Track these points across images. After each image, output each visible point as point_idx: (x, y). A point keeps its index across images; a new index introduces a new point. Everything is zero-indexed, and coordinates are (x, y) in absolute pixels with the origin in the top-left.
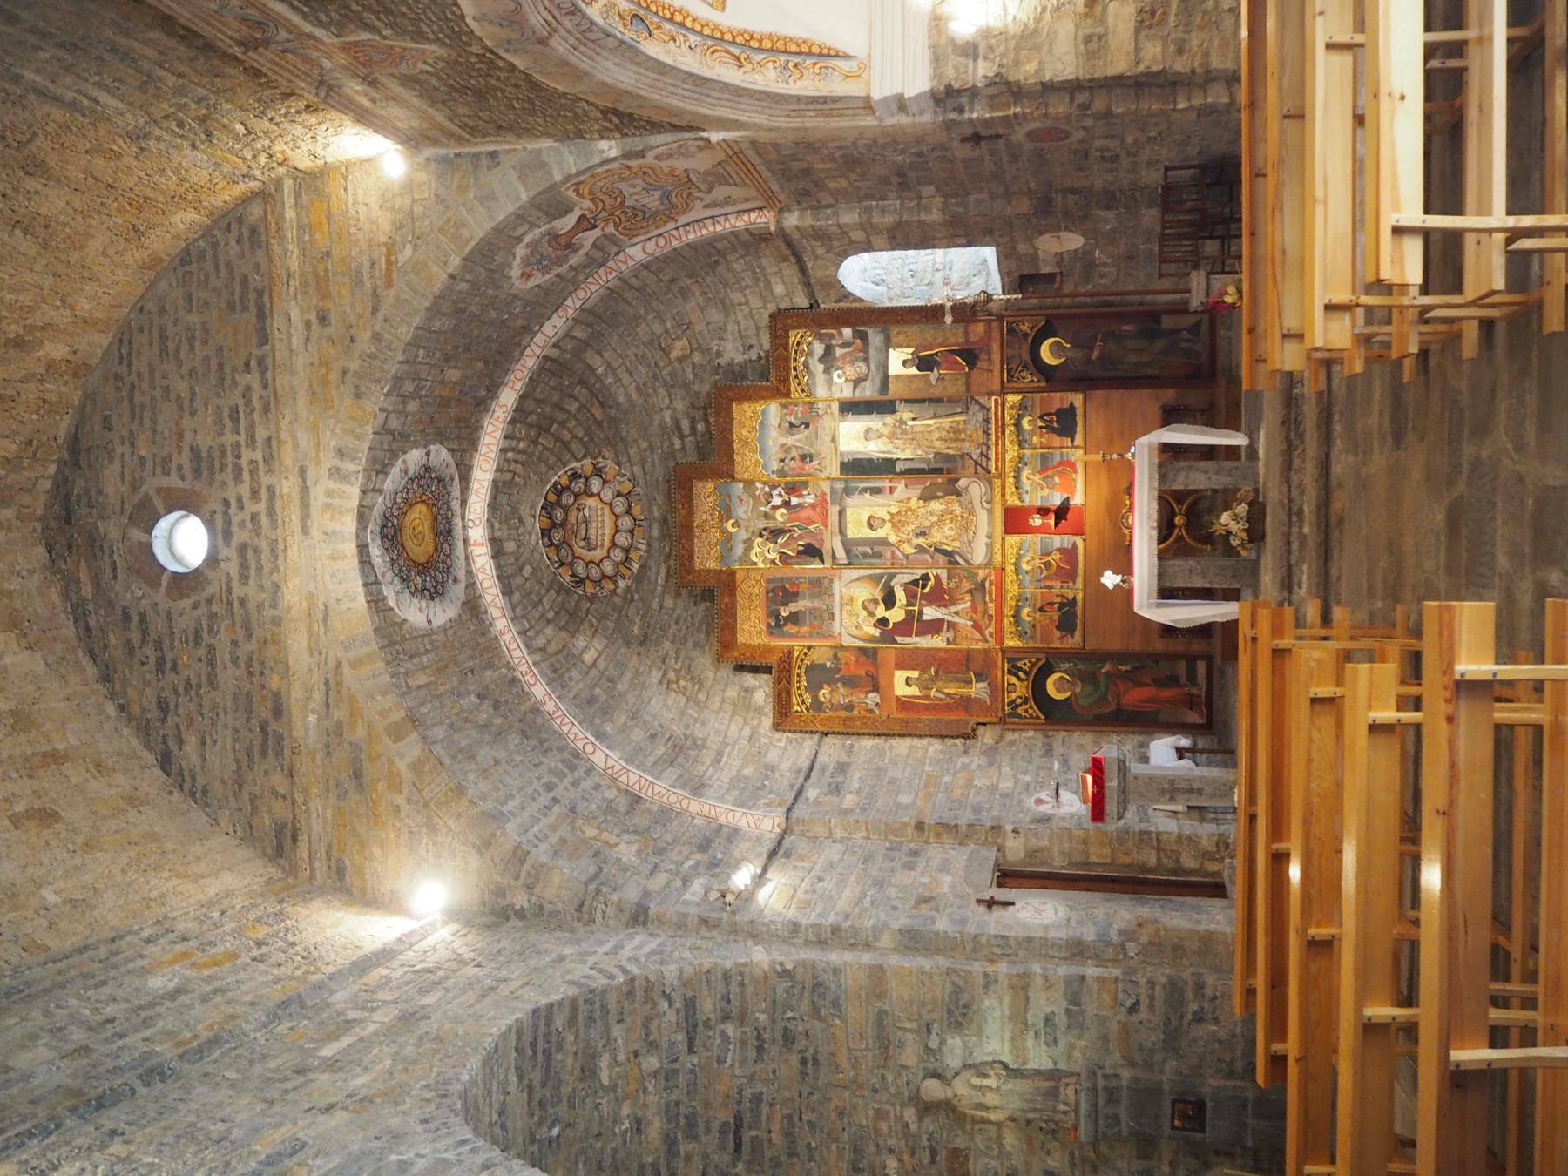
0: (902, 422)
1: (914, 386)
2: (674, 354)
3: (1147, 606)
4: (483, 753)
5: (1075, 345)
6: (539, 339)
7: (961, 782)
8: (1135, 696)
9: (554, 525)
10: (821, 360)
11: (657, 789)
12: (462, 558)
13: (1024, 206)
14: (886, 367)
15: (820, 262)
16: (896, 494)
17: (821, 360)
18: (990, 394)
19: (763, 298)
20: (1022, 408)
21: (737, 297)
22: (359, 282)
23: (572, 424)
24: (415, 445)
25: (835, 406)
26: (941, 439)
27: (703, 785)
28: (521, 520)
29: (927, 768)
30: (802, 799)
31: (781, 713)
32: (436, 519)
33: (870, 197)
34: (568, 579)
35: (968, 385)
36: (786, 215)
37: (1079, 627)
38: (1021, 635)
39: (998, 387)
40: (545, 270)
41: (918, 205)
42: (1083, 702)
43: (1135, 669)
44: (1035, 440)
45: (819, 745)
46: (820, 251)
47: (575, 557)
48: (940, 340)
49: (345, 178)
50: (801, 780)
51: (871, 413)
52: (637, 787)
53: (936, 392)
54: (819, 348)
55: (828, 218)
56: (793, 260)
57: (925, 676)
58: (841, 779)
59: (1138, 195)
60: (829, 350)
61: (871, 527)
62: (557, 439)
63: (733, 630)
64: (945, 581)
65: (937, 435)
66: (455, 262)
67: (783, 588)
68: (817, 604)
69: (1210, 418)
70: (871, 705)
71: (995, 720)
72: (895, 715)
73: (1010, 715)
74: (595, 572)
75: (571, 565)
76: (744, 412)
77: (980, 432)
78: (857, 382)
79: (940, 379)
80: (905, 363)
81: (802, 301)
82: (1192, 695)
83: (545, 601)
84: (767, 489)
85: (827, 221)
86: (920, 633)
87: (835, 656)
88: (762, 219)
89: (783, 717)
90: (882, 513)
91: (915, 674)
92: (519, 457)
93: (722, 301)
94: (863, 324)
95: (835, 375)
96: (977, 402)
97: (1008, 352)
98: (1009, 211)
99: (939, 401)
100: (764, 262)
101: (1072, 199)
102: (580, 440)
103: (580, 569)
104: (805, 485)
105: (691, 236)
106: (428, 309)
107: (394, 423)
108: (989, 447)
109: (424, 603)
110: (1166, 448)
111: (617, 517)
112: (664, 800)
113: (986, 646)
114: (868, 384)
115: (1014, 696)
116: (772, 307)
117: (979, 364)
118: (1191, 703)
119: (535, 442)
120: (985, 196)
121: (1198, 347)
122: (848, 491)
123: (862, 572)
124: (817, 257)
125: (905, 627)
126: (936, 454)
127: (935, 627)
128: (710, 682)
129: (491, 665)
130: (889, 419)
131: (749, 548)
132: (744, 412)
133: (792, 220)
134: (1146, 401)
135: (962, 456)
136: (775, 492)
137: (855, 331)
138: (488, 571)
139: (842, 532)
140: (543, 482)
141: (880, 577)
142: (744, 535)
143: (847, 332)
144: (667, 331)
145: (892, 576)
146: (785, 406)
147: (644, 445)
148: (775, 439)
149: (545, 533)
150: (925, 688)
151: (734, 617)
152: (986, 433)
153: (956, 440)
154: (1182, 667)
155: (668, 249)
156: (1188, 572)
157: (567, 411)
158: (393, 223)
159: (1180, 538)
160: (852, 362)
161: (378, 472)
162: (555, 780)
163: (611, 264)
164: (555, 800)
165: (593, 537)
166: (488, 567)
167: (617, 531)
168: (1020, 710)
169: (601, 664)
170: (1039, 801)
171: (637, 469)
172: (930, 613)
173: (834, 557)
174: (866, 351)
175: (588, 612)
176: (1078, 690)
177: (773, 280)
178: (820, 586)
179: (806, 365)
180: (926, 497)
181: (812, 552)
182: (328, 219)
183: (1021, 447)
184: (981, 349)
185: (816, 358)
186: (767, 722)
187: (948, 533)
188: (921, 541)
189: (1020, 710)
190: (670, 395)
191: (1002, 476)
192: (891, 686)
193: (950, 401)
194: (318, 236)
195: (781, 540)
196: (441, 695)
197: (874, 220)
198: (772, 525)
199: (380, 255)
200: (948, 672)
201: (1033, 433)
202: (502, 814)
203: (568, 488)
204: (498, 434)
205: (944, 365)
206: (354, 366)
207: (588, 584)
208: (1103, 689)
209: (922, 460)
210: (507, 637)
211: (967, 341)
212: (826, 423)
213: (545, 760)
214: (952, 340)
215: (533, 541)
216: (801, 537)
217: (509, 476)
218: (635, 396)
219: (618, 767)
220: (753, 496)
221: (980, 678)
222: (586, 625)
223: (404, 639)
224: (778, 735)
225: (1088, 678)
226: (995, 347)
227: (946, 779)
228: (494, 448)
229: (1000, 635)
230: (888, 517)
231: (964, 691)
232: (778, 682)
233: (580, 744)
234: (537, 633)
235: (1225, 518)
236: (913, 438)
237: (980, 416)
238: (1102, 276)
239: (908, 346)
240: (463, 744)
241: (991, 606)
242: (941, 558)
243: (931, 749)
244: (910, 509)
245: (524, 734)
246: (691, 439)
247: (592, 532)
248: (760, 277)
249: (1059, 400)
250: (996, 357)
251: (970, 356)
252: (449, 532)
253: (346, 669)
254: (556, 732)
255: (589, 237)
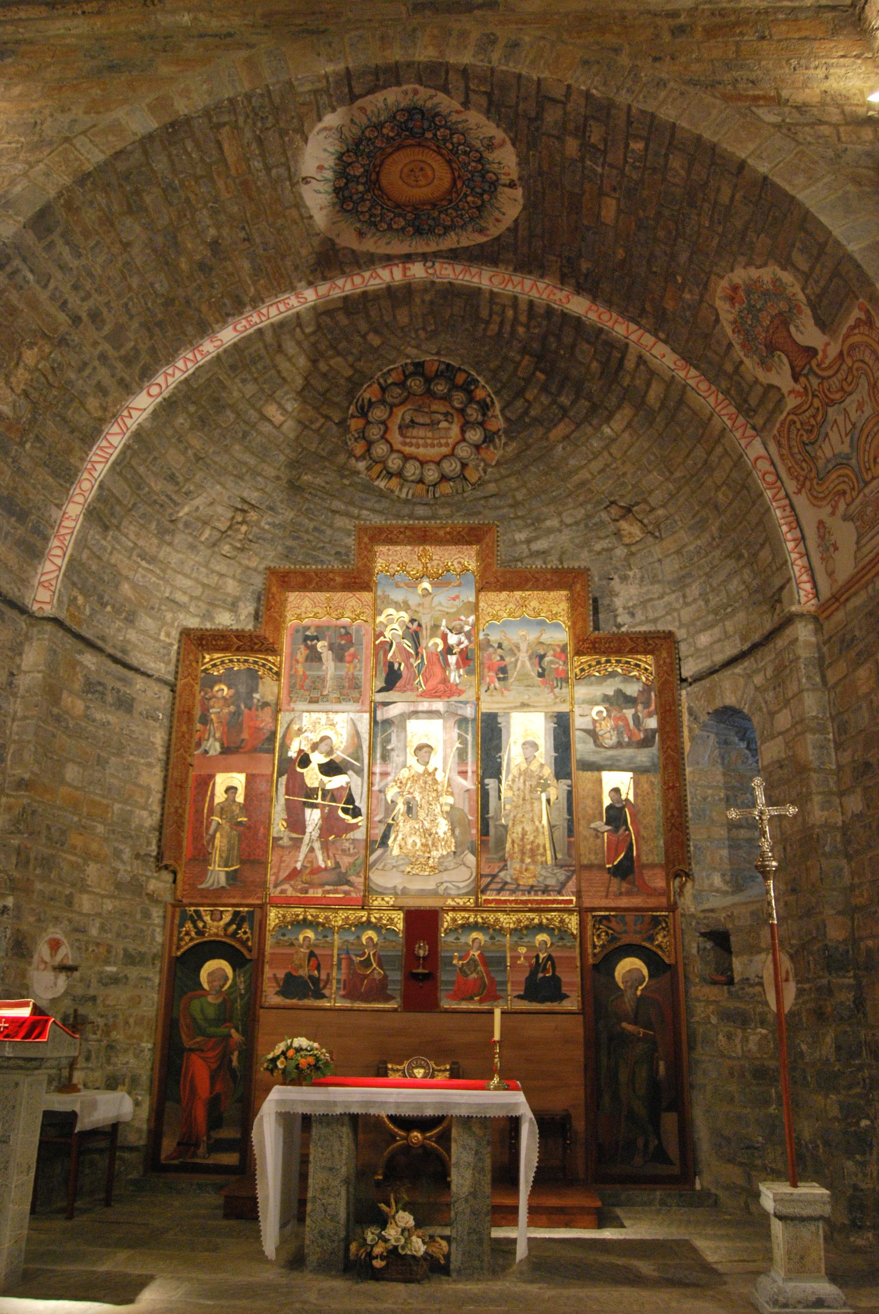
0: (545, 787)
1: (589, 802)
2: (623, 524)
3: (277, 1100)
4: (138, 229)
5: (640, 1000)
6: (648, 339)
7: (94, 846)
8: (199, 1071)
9: (428, 381)
10: (619, 692)
11: (99, 467)
12: (388, 250)
13: (836, 933)
14: (611, 768)
15: (742, 681)
16: (460, 780)
17: (619, 692)
18: (579, 894)
19: (693, 623)
20: (562, 932)
21: (694, 590)
22: (729, 66)
23: (545, 400)
24: (523, 161)
25: (564, 708)
26: (524, 833)
27: (106, 528)
28: (434, 334)
29: (117, 806)
30: (81, 646)
31: (201, 639)
32: (434, 206)
33: (842, 729)
34: (367, 396)
35: (589, 867)
36: (811, 627)
37: (288, 1002)
38: (282, 928)
39: (587, 903)
40: (739, 326)
41: (831, 793)
42: (196, 1005)
43: (232, 1071)
44: (523, 950)
45: (159, 680)
46: (758, 680)
47: (392, 407)
48: (643, 833)
49: (857, 57)
50: (111, 651)
51: (556, 749)
52: (104, 444)
53: (581, 829)
54: (632, 690)
55: (809, 678)
56: (745, 647)
57: (237, 811)
58: (110, 699)
59: (857, 1090)
60: (631, 701)
61: (419, 748)
62: (528, 380)
63: (303, 587)
64: (351, 835)
65: (529, 828)
66: (763, 168)
67: (350, 643)
68: (329, 683)
69: (544, 1179)
70: (206, 745)
71: (179, 894)
72: (192, 773)
73: (184, 912)
74: (374, 432)
75: (383, 402)
76: (557, 603)
77: (531, 882)
78: (592, 733)
79: (597, 834)
80: (616, 791)
81: (689, 669)
82: (197, 1145)
83: (339, 359)
84: (467, 628)
85: (804, 675)
86: (289, 805)
87: (266, 704)
88: (803, 598)
89: (200, 641)
90: (436, 761)
91: (240, 798)
92: (507, 328)
93: (689, 575)
94: (662, 741)
95: (601, 708)
96: (569, 878)
97: (630, 917)
98: (829, 911)
99: (570, 831)
100: (741, 616)
101: (846, 997)
102: (526, 412)
103: (378, 413)
104: (470, 673)
105: (778, 513)
106: (699, 138)
107: (552, 115)
108: (513, 892)
109: (329, 175)
110: (514, 1123)
111: (438, 463)
112: (86, 475)
113: (271, 886)
114: (591, 746)
115: (207, 918)
116: (681, 634)
117: (615, 881)
118: (187, 1144)
119: (524, 351)
120: (847, 880)
121: (638, 1160)
122: (462, 722)
123: (365, 736)
124: (749, 676)
125: (297, 786)
126: (505, 827)
127: (296, 824)
128: (245, 562)
129: (257, 271)
130: (548, 772)
131: (398, 607)
132: (557, 603)
133: (804, 632)
134: (570, 1097)
135: (503, 859)
136: (463, 638)
137: (654, 731)
138: (372, 282)
139: (415, 714)
140: (476, 365)
141: (358, 759)
142: (413, 601)
143: (652, 723)
144: (653, 510)
145: (359, 772)
146: (564, 648)
147: (519, 496)
148: (523, 638)
149: (419, 366)
150: (223, 810)
151: (319, 589)
152: (531, 889)
153: (523, 853)
154: (228, 1133)
155: (762, 485)
156: (334, 1164)
157: (559, 394)
158: (805, 105)
159: (393, 1137)
160: (616, 727)
161: (489, 95)
162: (107, 329)
163: (741, 420)
164: (76, 320)
165: (415, 432)
166: (378, 281)
167: (422, 463)
168: (189, 925)
169: (266, 428)
170: (55, 945)
171: (492, 488)
172: (313, 817)
173: (386, 704)
174: (629, 745)
175: (328, 418)
176: (210, 999)
177: (717, 631)
178: (350, 689)
179: (613, 674)
180: (452, 815)
181: (392, 679)
182: (805, 38)
183: (513, 931)
184: (632, 883)
185: (621, 686)
186: (193, 623)
187: (410, 841)
188: (401, 807)
189: (189, 925)
190: (577, 523)
191: (477, 909)
192: (228, 769)
193: (570, 845)
194: (784, 28)
195: (407, 644)
196: (212, 181)
197: (810, 737)
198: (424, 633)
199: (767, 88)
200: (240, 836)
201: (531, 947)
202: (50, 231)
203: (471, 399)
204: (534, 294)
205: (614, 838)
206: (624, 60)
207: (360, 423)
208: (212, 1030)
209: (498, 810)
210: (293, 301)
211: (644, 866)
212: (545, 696)
213: (135, 325)
214: (645, 848)
215: (410, 350)
216: (409, 666)
217: (484, 313)
218: (576, 479)
219: (129, 422)
220: (458, 612)
221: (232, 877)
222: (311, 413)
223: (283, 133)
224: (175, 633)
225: (224, 1014)
226: (637, 901)
227: (100, 829)
228: (518, 289)
229: (286, 903)
230: (430, 769)
231: (216, 857)
232: (240, 635)
233: (160, 379)
234: (299, 343)
235: (406, 1219)
236: (527, 799)
237: (552, 882)
238: (729, 1037)
239: (636, 795)
240: (148, 199)
241: (319, 893)
242: (378, 832)
243: (145, 814)
244: (439, 795)
245: (169, 302)
246: (526, 552)
247: (421, 432)
248: (720, 614)
249: (571, 979)
250: (624, 902)
251: (625, 870)
252: (419, 232)
253: (244, 54)
254: (176, 351)
255: (781, 378)
